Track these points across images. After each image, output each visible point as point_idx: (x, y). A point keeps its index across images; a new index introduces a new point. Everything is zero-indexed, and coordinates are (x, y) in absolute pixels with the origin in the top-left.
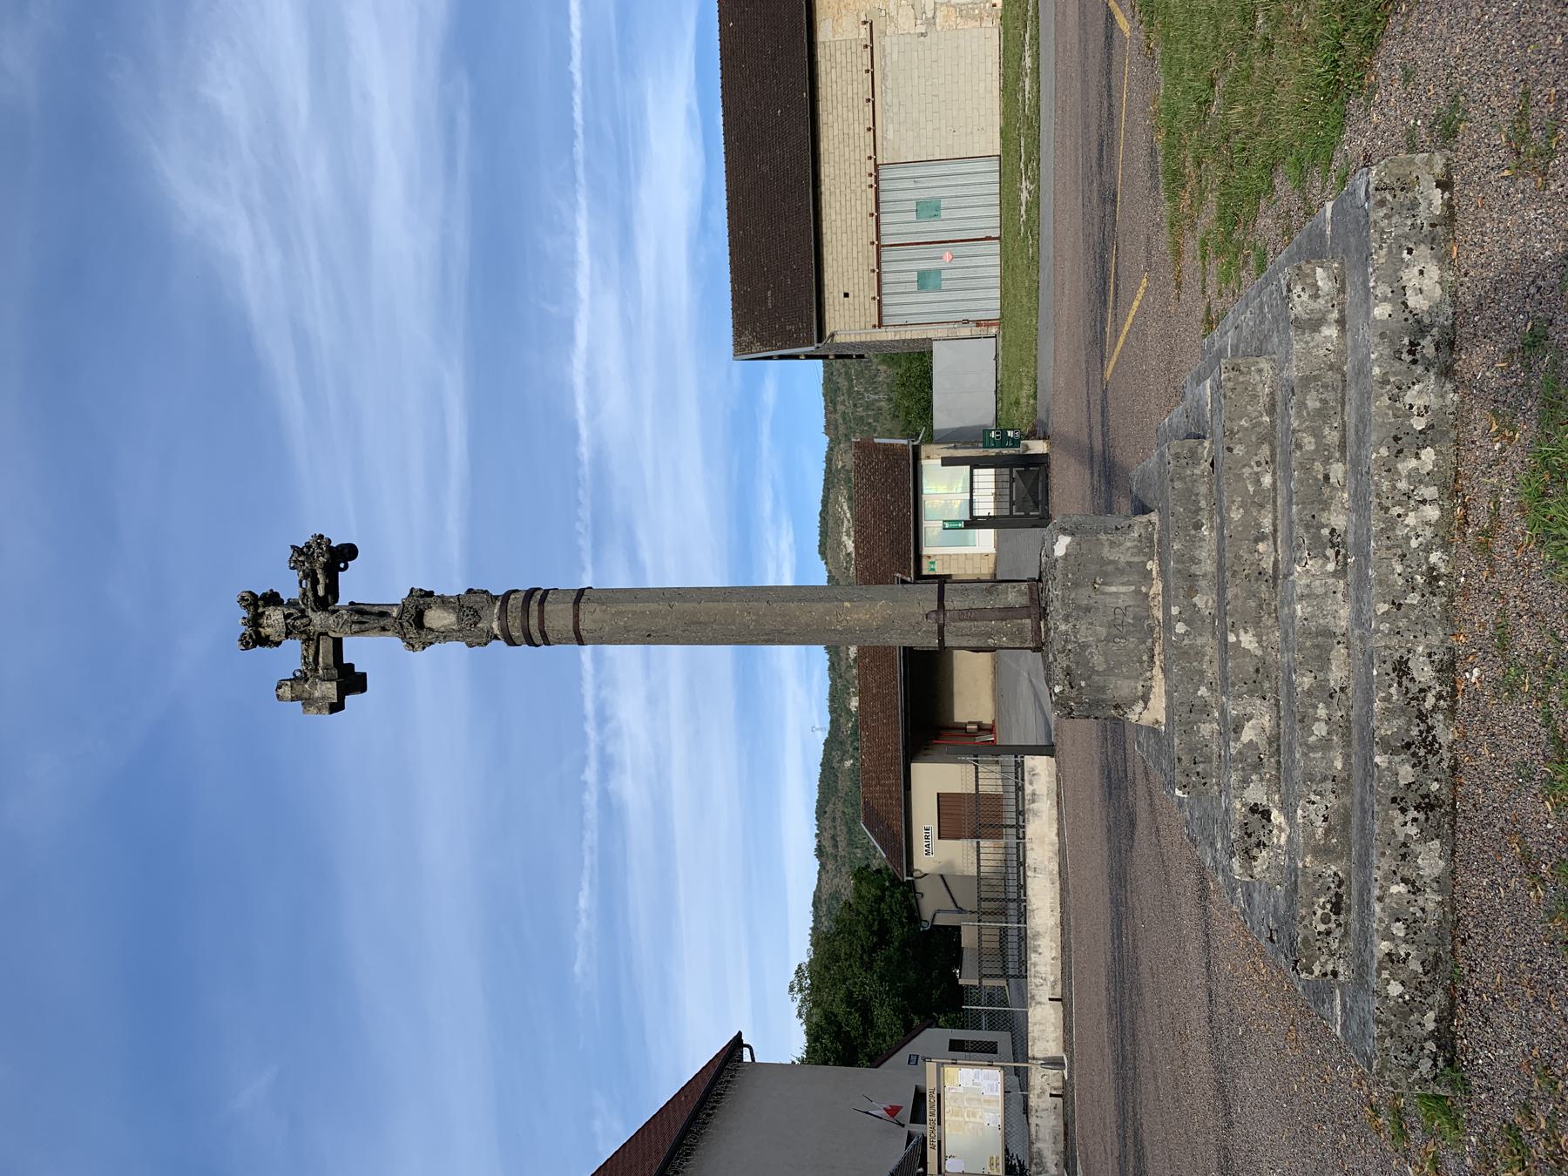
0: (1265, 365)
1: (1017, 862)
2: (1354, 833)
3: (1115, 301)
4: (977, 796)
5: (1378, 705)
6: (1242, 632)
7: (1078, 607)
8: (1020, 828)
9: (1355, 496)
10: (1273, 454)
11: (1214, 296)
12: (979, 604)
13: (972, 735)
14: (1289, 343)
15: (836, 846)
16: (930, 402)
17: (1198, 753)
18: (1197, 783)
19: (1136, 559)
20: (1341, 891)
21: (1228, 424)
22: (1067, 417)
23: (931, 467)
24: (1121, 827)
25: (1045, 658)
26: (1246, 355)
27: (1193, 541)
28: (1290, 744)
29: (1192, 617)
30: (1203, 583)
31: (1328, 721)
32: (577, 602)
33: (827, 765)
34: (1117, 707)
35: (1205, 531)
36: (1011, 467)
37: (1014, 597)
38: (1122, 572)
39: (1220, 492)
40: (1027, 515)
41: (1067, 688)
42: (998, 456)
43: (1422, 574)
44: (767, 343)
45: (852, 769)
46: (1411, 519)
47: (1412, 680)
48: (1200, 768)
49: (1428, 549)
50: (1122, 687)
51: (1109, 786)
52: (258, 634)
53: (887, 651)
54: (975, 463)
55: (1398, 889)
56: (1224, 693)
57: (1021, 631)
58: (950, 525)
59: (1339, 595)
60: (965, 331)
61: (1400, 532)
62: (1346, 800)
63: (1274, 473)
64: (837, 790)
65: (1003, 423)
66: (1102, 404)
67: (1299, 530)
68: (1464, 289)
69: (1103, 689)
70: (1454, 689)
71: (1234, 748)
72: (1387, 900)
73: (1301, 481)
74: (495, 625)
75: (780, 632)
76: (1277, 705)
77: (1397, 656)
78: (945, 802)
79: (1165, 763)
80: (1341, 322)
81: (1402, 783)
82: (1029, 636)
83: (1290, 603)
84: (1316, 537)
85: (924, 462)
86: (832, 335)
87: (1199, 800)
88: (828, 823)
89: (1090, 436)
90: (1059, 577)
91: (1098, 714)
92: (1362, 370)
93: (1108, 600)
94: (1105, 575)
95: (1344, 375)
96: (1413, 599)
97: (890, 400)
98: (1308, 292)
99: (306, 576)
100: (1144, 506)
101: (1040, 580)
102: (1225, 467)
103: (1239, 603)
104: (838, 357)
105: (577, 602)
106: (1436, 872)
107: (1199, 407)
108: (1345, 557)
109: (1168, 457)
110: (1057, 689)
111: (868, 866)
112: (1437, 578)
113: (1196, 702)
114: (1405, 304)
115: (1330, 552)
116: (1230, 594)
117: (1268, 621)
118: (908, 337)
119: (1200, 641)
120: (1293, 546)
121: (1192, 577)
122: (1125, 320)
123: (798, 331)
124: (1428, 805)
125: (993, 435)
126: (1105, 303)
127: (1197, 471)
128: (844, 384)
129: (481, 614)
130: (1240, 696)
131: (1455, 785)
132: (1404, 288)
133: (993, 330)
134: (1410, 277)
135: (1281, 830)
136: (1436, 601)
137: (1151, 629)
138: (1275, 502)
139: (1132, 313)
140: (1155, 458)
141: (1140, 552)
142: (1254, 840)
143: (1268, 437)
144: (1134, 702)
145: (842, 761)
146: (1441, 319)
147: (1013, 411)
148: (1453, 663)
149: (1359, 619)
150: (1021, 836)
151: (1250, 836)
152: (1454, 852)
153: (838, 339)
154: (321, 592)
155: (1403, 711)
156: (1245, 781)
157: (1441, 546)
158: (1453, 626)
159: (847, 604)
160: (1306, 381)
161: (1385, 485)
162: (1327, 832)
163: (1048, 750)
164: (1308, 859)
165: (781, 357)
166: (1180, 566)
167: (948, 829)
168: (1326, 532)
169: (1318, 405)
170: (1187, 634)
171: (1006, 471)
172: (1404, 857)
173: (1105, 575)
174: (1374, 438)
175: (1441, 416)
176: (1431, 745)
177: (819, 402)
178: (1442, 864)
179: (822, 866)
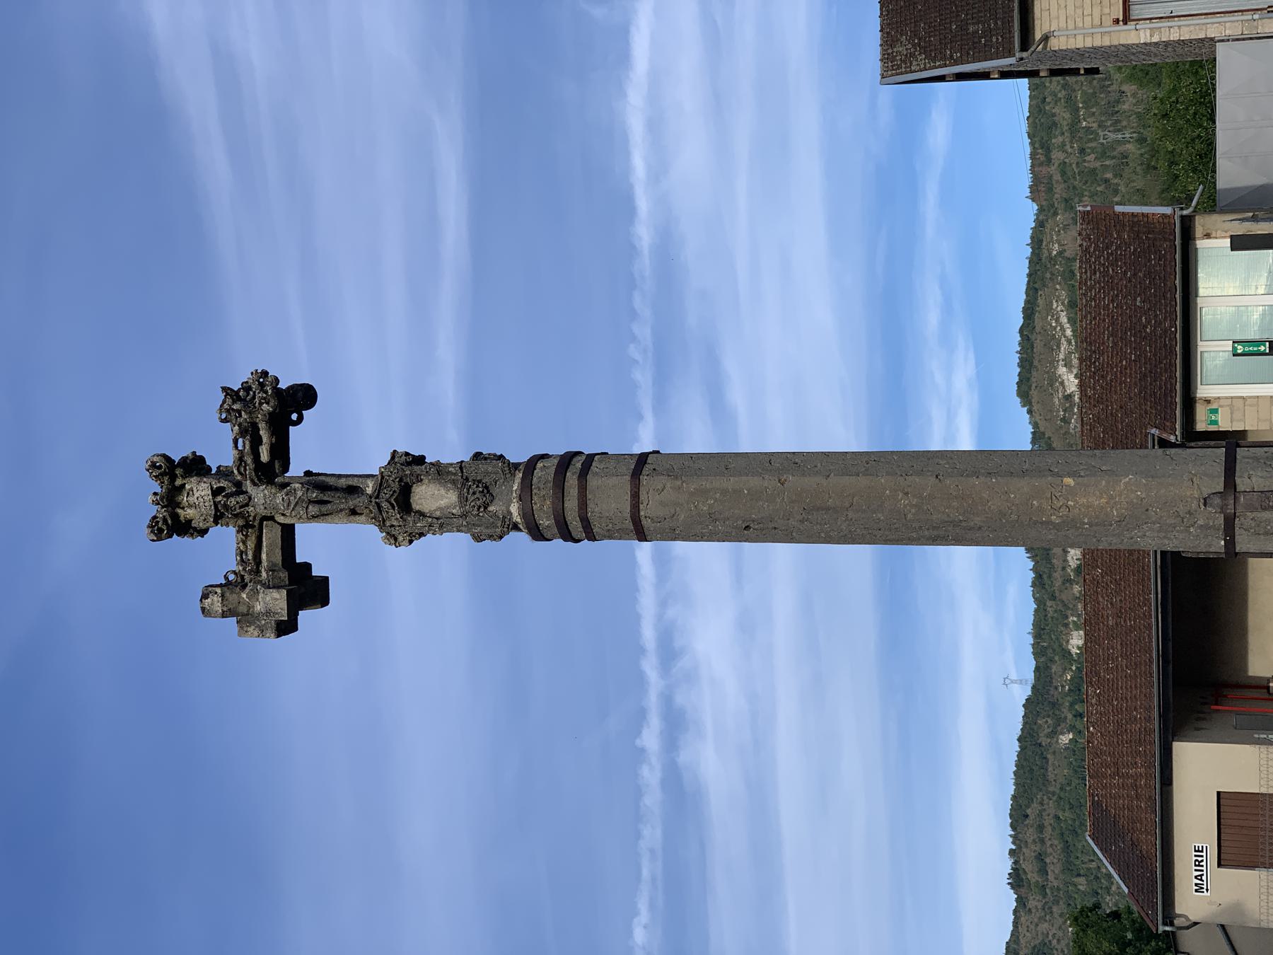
15: (1043, 871)
33: (1028, 738)
44: (936, 54)
45: (1073, 747)
52: (175, 517)
53: (1134, 557)
58: (1246, 349)
64: (1046, 781)
74: (514, 509)
75: (956, 524)
85: (1201, 244)
86: (1046, 38)
88: (1031, 834)
97: (1142, 140)
99: (243, 433)
104: (1054, 73)
111: (1097, 906)
118: (1174, 36)
123: (988, 33)
129: (495, 491)
145: (1054, 734)
153: (1055, 44)
154: (265, 456)
159: (1069, 481)
179: (1021, 901)
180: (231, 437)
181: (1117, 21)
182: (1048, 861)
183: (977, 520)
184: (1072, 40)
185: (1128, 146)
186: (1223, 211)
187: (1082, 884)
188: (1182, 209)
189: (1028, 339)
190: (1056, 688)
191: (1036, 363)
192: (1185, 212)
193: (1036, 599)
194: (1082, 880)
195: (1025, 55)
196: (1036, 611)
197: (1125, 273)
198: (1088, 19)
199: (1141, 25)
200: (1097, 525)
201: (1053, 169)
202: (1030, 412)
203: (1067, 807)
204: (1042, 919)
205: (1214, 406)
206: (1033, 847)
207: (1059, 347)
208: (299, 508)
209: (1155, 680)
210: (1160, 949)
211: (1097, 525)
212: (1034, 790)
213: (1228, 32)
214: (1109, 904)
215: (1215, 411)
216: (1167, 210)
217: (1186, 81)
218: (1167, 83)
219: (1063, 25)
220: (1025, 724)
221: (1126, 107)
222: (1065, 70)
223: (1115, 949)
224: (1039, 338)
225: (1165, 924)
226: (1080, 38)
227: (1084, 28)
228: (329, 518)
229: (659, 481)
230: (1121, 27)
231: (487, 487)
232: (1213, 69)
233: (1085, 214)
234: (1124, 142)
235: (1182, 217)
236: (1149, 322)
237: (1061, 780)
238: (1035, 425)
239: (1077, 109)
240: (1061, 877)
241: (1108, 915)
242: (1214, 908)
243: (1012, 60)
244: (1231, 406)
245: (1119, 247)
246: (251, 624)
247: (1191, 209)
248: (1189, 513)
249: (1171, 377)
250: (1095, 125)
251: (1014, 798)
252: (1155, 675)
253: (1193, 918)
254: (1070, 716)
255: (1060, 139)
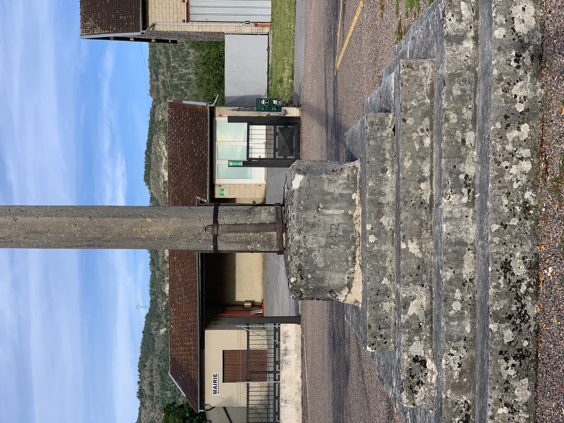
0: (428, 64)
1: (274, 397)
2: (477, 374)
3: (343, 16)
4: (248, 352)
5: (491, 291)
6: (409, 242)
7: (307, 224)
8: (276, 373)
9: (480, 154)
10: (431, 125)
11: (403, 16)
12: (241, 221)
13: (248, 310)
14: (443, 51)
15: (152, 390)
16: (223, 77)
17: (381, 322)
18: (380, 341)
19: (346, 192)
20: (469, 413)
21: (403, 103)
22: (312, 92)
23: (221, 122)
24: (341, 371)
25: (286, 258)
26: (418, 57)
27: (381, 181)
28: (438, 316)
29: (379, 231)
30: (387, 209)
31: (462, 301)
33: (147, 332)
34: (331, 292)
35: (389, 174)
36: (275, 125)
37: (265, 216)
38: (336, 200)
39: (398, 148)
40: (285, 158)
41: (299, 279)
42: (268, 117)
43: (520, 206)
44: (105, 27)
45: (165, 335)
46: (514, 170)
47: (513, 274)
48: (383, 332)
49: (523, 189)
50: (335, 278)
51: (334, 344)
53: (188, 253)
54: (251, 121)
55: (503, 410)
56: (398, 282)
57: (270, 239)
58: (233, 164)
59: (470, 219)
60: (248, 29)
61: (507, 178)
62: (473, 353)
63: (432, 137)
64: (154, 350)
65: (272, 94)
66: (333, 84)
67: (446, 175)
68: (548, 22)
69: (322, 280)
70: (538, 280)
71: (404, 318)
72: (496, 418)
73: (447, 143)
75: (99, 239)
76: (431, 290)
77: (503, 259)
78: (228, 356)
79: (361, 329)
80: (475, 38)
81: (506, 341)
82: (275, 243)
83: (439, 223)
84: (456, 180)
85: (218, 119)
86: (154, 25)
87: (383, 354)
88: (147, 374)
89: (326, 107)
90: (295, 203)
91: (319, 296)
92: (487, 72)
93: (327, 219)
94: (325, 202)
95: (476, 74)
96: (514, 222)
97: (196, 74)
98: (456, 17)
100: (352, 155)
101: (283, 205)
102: (401, 132)
103: (409, 222)
104: (158, 41)
106: (526, 399)
107: (387, 91)
108: (474, 193)
109: (366, 124)
110: (292, 280)
111: (174, 403)
112: (528, 209)
113: (381, 288)
114: (513, 29)
115: (465, 190)
116: (402, 217)
117: (426, 235)
118: (208, 30)
119: (384, 248)
120: (442, 186)
121: (380, 205)
122: (349, 29)
123: (128, 20)
124: (521, 355)
125: (263, 102)
126: (337, 16)
127: (384, 134)
128: (163, 60)
130: (408, 284)
131: (537, 342)
132: (513, 18)
133: (267, 30)
134: (517, 11)
135: (433, 373)
136: (528, 223)
137: (354, 239)
138: (432, 156)
139: (353, 24)
140: (359, 124)
141: (348, 187)
142: (415, 380)
143: (428, 114)
144: (340, 289)
145: (158, 329)
146: (535, 40)
147: (279, 86)
148: (537, 264)
149: (481, 235)
150: (277, 379)
151: (413, 377)
152: (536, 386)
153: (157, 28)
155: (507, 294)
156: (410, 341)
157: (531, 188)
158: (538, 240)
159: (149, 220)
160: (453, 77)
161: (499, 147)
162: (461, 374)
163: (296, 319)
164: (449, 392)
165: (116, 38)
166: (373, 198)
167: (229, 376)
168: (462, 177)
169: (459, 93)
170: (376, 243)
171: (272, 127)
172: (506, 389)
173: (325, 202)
174: (492, 116)
175: (533, 103)
176: (523, 316)
177: (147, 73)
178: (529, 393)
179: (142, 404)
181: (184, 21)
182: (154, 385)
183: (108, 237)
184: (165, 27)
185: (191, 76)
186: (228, 106)
187: (169, 394)
188: (210, 104)
189: (149, 156)
190: (159, 309)
191: (152, 167)
192: (211, 105)
193: (151, 270)
194: (169, 392)
195: (144, 32)
196: (151, 276)
197: (187, 130)
198: (172, 19)
199: (194, 24)
200: (161, 239)
201: (159, 83)
202: (149, 188)
203: (163, 360)
204: (151, 411)
205: (222, 187)
206: (148, 380)
207: (162, 161)
209: (198, 304)
210: (200, 419)
211: (161, 239)
212: (149, 354)
213: (230, 30)
214: (180, 401)
215: (223, 190)
216: (204, 104)
217: (213, 50)
218: (207, 50)
219: (161, 20)
220: (146, 325)
221: (190, 59)
222: (162, 40)
223: (181, 421)
224: (153, 156)
225: (201, 409)
226: (168, 27)
227: (170, 22)
230: (186, 24)
232: (224, 46)
233: (170, 104)
234: (189, 74)
235: (210, 107)
236: (196, 151)
237: (161, 349)
238: (152, 194)
239: (170, 58)
240: (160, 391)
241: (179, 407)
242: (221, 400)
243: (139, 34)
244: (229, 188)
245: (184, 119)
247: (214, 104)
248: (199, 234)
249: (205, 175)
250: (177, 65)
251: (140, 358)
252: (198, 302)
253: (212, 406)
254: (165, 321)
255: (162, 70)
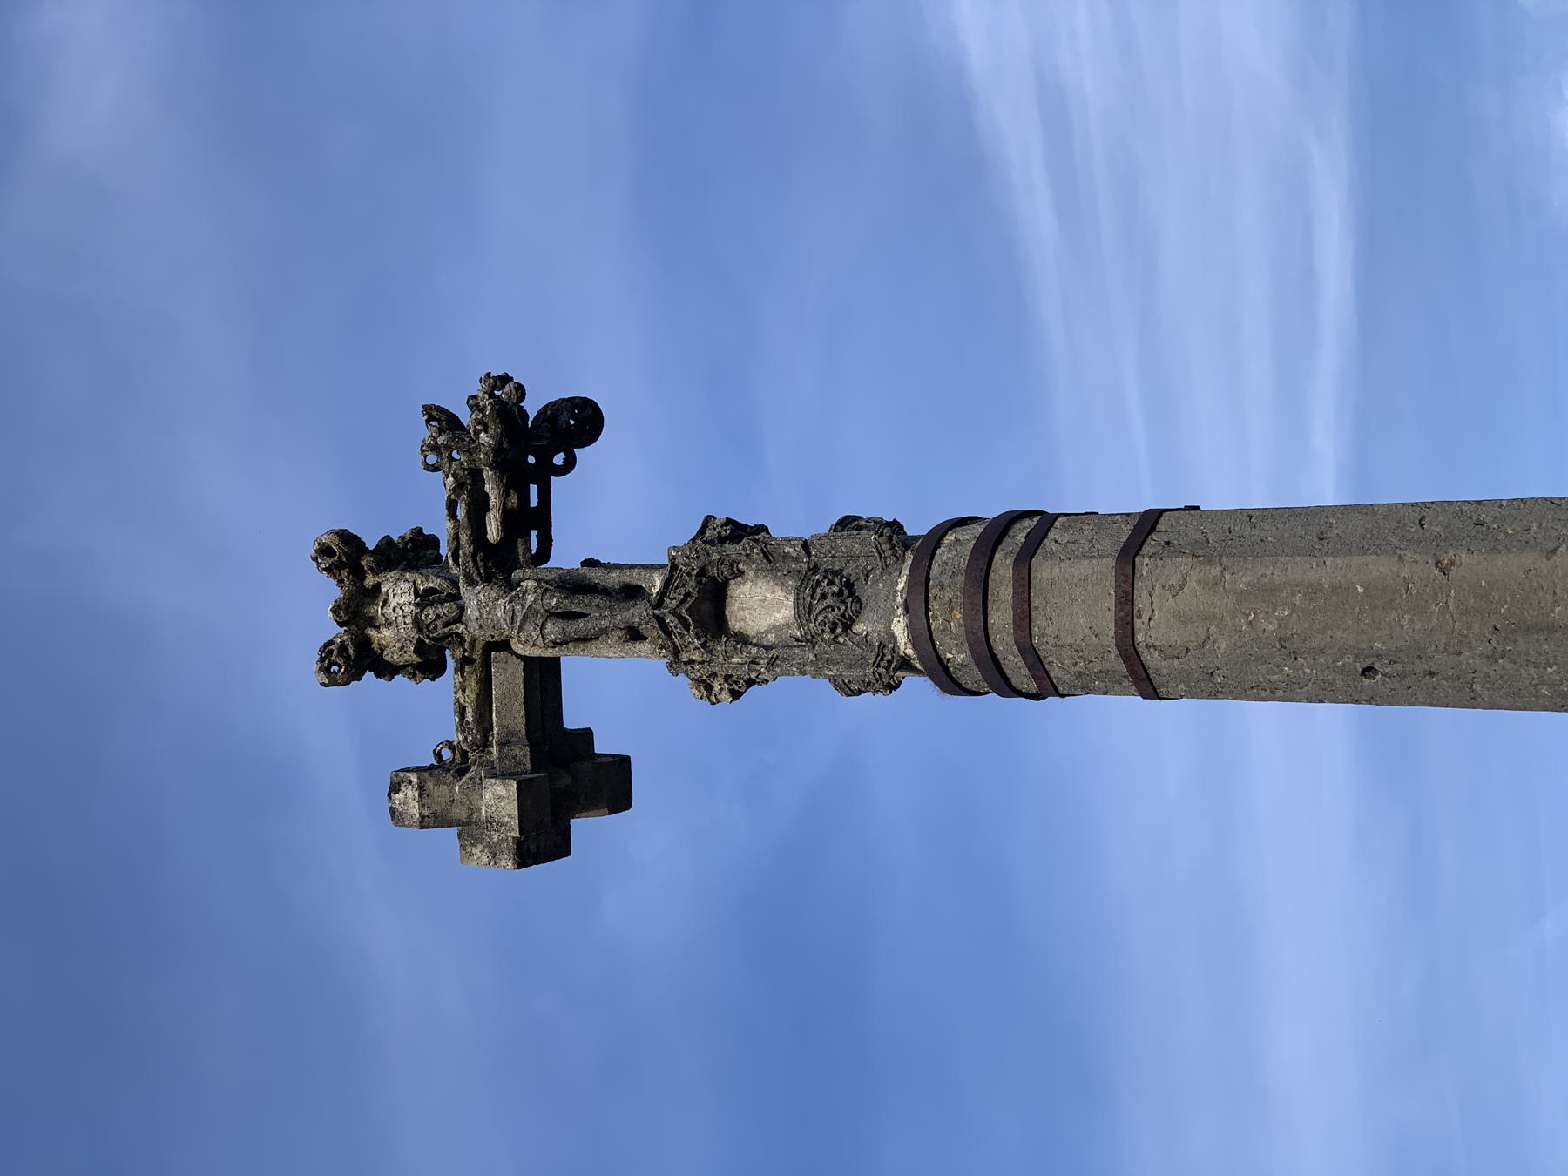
32: (1129, 554)
52: (364, 644)
74: (899, 628)
99: (459, 487)
105: (1129, 554)
129: (865, 591)
154: (493, 533)
180: (443, 496)
208: (529, 627)
228: (592, 646)
229: (1174, 568)
231: (849, 585)
246: (477, 840)
